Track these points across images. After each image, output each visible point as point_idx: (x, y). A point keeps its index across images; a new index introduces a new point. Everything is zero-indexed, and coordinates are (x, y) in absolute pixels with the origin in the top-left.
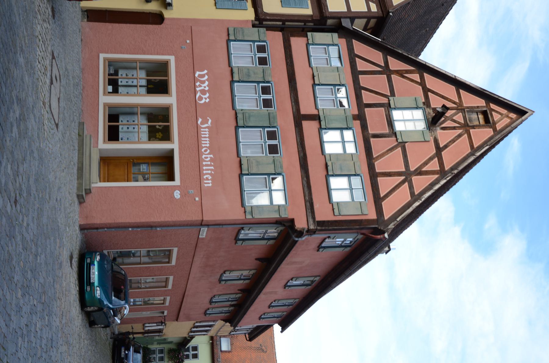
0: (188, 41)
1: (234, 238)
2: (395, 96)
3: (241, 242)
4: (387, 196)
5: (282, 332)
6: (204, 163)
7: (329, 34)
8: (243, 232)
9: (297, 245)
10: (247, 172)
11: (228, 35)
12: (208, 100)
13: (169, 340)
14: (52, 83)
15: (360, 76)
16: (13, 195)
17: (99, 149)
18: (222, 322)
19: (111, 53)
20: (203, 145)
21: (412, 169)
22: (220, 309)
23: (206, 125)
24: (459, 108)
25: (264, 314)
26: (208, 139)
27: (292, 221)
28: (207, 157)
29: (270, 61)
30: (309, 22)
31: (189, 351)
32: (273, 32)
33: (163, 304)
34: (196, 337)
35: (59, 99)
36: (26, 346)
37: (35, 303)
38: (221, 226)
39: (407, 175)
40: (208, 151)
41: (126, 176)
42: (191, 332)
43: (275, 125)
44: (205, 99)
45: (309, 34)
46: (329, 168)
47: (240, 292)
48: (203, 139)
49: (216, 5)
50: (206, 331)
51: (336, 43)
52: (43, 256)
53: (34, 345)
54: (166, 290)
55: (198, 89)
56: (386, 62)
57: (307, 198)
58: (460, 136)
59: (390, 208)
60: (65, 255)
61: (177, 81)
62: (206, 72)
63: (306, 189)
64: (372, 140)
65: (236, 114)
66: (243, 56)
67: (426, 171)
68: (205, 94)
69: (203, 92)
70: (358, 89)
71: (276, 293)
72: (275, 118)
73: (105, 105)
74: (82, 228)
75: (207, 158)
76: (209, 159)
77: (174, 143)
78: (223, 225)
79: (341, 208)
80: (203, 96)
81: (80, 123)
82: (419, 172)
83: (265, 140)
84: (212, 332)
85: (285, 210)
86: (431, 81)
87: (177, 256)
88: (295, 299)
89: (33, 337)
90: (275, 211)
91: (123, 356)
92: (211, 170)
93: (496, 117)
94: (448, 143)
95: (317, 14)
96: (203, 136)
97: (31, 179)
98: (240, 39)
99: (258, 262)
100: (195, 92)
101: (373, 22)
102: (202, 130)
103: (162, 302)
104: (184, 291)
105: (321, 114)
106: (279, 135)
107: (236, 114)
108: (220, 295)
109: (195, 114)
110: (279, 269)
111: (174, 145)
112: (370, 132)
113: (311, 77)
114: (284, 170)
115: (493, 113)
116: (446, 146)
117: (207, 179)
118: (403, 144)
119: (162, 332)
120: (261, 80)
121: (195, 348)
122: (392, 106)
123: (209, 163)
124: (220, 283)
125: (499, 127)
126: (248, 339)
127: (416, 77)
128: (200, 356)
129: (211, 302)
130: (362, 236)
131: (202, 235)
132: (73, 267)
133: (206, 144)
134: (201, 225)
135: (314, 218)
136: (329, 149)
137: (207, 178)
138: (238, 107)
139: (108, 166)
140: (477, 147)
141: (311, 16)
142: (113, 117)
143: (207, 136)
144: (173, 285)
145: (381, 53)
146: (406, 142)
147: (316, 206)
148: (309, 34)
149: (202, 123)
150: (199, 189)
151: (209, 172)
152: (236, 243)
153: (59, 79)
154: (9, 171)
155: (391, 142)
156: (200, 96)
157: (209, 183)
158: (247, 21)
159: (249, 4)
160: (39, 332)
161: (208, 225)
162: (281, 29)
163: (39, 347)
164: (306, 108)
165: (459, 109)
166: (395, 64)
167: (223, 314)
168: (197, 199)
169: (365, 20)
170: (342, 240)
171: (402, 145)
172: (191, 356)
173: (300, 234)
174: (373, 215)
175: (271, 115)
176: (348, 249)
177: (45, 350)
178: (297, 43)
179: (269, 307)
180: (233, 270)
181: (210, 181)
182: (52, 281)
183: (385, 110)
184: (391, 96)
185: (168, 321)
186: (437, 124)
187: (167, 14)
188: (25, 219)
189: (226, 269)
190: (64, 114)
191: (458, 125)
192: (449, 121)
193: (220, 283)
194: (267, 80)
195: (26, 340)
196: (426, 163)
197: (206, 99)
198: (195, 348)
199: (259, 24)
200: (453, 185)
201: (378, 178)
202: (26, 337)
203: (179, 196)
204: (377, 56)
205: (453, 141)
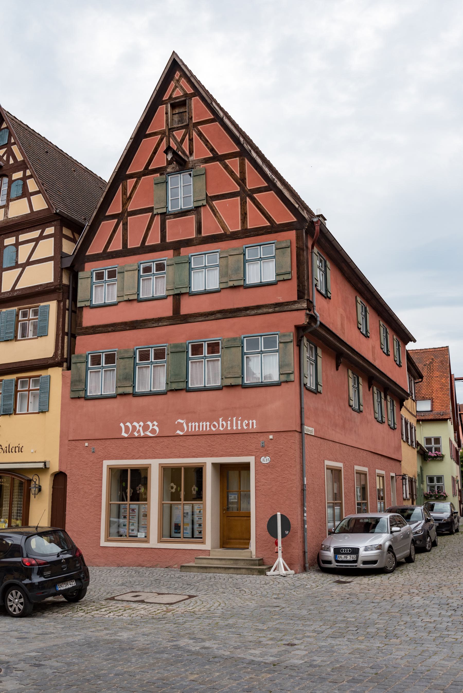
1: (315, 395)
2: (153, 207)
3: (319, 386)
4: (268, 218)
5: (415, 341)
6: (229, 428)
7: (80, 281)
8: (308, 385)
9: (323, 322)
12: (155, 423)
13: (419, 470)
14: (142, 602)
15: (129, 247)
16: (284, 648)
18: (403, 409)
19: (100, 533)
20: (208, 429)
21: (238, 189)
22: (389, 411)
23: (185, 425)
25: (395, 361)
27: (298, 328)
28: (222, 425)
29: (109, 351)
30: (65, 305)
31: (431, 448)
33: (383, 477)
34: (417, 439)
36: (453, 633)
37: (402, 623)
40: (215, 423)
41: (242, 518)
42: (412, 445)
44: (154, 426)
45: (79, 305)
46: (235, 285)
47: (371, 389)
49: (45, 412)
50: (411, 428)
51: (90, 274)
52: (347, 615)
53: (450, 624)
54: (369, 474)
55: (142, 434)
56: (113, 217)
57: (271, 310)
58: (200, 134)
59: (284, 216)
60: (336, 588)
61: (133, 458)
62: (122, 425)
63: (260, 311)
64: (203, 235)
65: (172, 390)
66: (101, 382)
67: (240, 173)
68: (148, 426)
69: (146, 428)
71: (373, 348)
72: (176, 346)
73: (160, 541)
74: (305, 569)
75: (223, 425)
76: (224, 423)
79: (283, 271)
80: (151, 428)
82: (241, 181)
84: (412, 420)
86: (136, 167)
88: (380, 325)
89: (441, 626)
90: (286, 347)
92: (237, 420)
93: (178, 93)
94: (208, 148)
95: (55, 295)
97: (260, 628)
99: (341, 367)
101: (66, 231)
102: (190, 430)
103: (381, 478)
104: (370, 453)
105: (171, 293)
106: (197, 341)
107: (172, 390)
108: (375, 412)
109: (172, 438)
110: (349, 343)
111: (208, 462)
112: (195, 237)
113: (129, 304)
114: (238, 336)
115: (174, 96)
116: (212, 150)
117: (248, 425)
118: (209, 199)
119: (412, 478)
121: (428, 440)
122: (164, 210)
123: (229, 422)
124: (362, 412)
125: (190, 91)
126: (420, 380)
128: (437, 435)
129: (382, 422)
130: (315, 247)
133: (206, 425)
134: (301, 432)
135: (294, 302)
136: (214, 284)
137: (246, 426)
138: (163, 387)
139: (231, 539)
140: (213, 115)
141: (59, 302)
144: (364, 466)
145: (102, 223)
147: (280, 299)
148: (79, 305)
149: (182, 430)
150: (259, 434)
151: (239, 422)
152: (320, 393)
153: (136, 593)
154: (257, 652)
155: (206, 213)
156: (149, 432)
157: (253, 423)
158: (63, 375)
160: (434, 618)
161: (302, 425)
162: (73, 337)
163: (451, 619)
164: (165, 309)
165: (169, 134)
166: (115, 207)
167: (395, 407)
168: (271, 437)
169: (64, 241)
170: (318, 270)
171: (210, 199)
172: (437, 446)
173: (313, 318)
175: (174, 350)
176: (328, 264)
177: (453, 612)
178: (89, 319)
179: (388, 355)
181: (251, 422)
182: (373, 604)
183: (169, 219)
185: (401, 472)
186: (186, 159)
187: (55, 468)
188: (308, 634)
189: (347, 405)
190: (176, 589)
191: (187, 136)
193: (362, 412)
194: (133, 355)
195: (447, 633)
196: (232, 173)
197: (154, 425)
200: (253, 143)
202: (443, 633)
203: (268, 457)
204: (106, 227)
205: (206, 142)
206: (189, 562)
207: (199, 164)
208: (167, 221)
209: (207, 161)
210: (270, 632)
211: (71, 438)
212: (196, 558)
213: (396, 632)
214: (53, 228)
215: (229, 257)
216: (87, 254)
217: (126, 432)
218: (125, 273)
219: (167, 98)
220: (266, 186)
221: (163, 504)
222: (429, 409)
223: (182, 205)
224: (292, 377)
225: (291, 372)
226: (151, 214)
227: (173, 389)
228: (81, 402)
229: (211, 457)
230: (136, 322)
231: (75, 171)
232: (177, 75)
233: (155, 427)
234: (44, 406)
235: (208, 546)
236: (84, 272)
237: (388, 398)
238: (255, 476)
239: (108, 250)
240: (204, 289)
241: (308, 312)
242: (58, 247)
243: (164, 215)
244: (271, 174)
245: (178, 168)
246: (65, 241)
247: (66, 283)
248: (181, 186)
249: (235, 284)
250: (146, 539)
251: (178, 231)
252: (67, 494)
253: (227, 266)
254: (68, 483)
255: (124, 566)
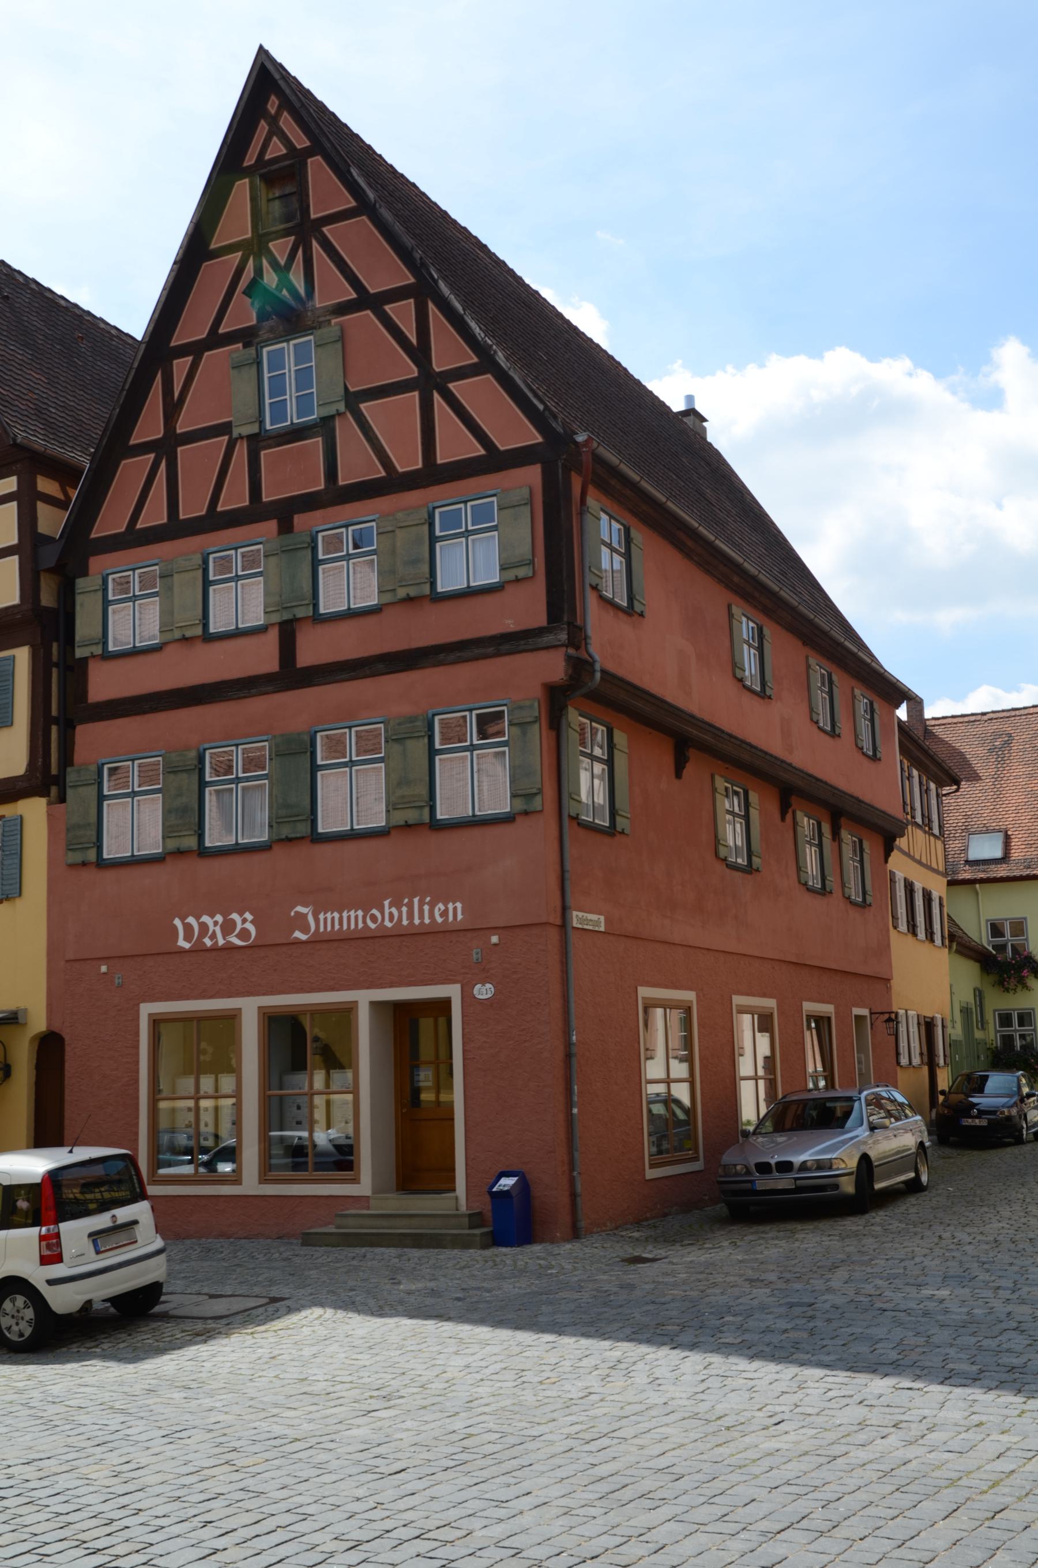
0: (104, 969)
2: (230, 423)
6: (405, 922)
7: (79, 599)
10: (426, 811)
11: (84, 864)
12: (248, 916)
15: (181, 517)
17: (373, 1193)
18: (895, 857)
20: (361, 925)
21: (414, 372)
23: (311, 919)
24: (255, 250)
26: (345, 914)
28: (389, 916)
32: (76, 747)
35: (212, 1296)
38: (567, 875)
39: (430, 383)
40: (374, 911)
43: (307, 738)
44: (245, 922)
45: (79, 653)
46: (412, 594)
47: (789, 816)
48: (345, 927)
55: (221, 942)
57: (490, 650)
61: (204, 995)
62: (177, 922)
68: (233, 923)
69: (228, 927)
70: (215, 521)
73: (264, 1179)
75: (391, 915)
76: (394, 910)
77: (356, 1002)
78: (563, 871)
81: (305, 1244)
82: (420, 353)
83: (231, 782)
85: (521, 708)
86: (191, 329)
87: (666, 987)
90: (524, 733)
91: (984, 1123)
92: (421, 904)
93: (277, 149)
96: (337, 927)
98: (94, 833)
99: (689, 770)
100: (230, 948)
101: (46, 485)
102: (322, 929)
105: (276, 618)
111: (249, 1009)
117: (444, 914)
120: (195, 778)
122: (254, 429)
123: (404, 909)
125: (302, 142)
127: (181, 366)
128: (1017, 914)
131: (597, 923)
132: (664, 1254)
133: (356, 917)
134: (564, 925)
135: (540, 632)
137: (441, 915)
138: (263, 836)
142: (299, 1158)
143: (336, 915)
144: (764, 995)
145: (123, 462)
146: (346, 388)
147: (510, 625)
148: (79, 653)
149: (305, 929)
151: (426, 908)
155: (346, 431)
156: (237, 936)
157: (455, 909)
158: (50, 816)
159: (6, 810)
161: (565, 910)
162: (68, 727)
164: (262, 656)
166: (149, 427)
168: (495, 939)
169: (41, 506)
171: (353, 400)
174: (532, 475)
178: (104, 684)
180: (716, 836)
181: (451, 906)
183: (266, 448)
184: (230, 433)
187: (38, 1023)
191: (300, 252)
192: (291, 276)
194: (195, 762)
197: (244, 921)
198: (996, 930)
199: (56, 784)
201: (439, 461)
203: (489, 986)
204: (132, 471)
206: (326, 1224)
207: (328, 318)
208: (262, 453)
209: (343, 309)
210: (368, 1374)
211: (70, 956)
212: (337, 1215)
213: (951, 1366)
214: (14, 479)
215: (398, 531)
216: (93, 536)
217: (186, 939)
218: (176, 576)
219: (253, 162)
220: (474, 364)
221: (269, 1096)
222: (998, 854)
223: (293, 417)
224: (537, 803)
225: (535, 791)
226: (226, 438)
227: (283, 837)
228: (89, 875)
229: (368, 988)
230: (203, 687)
231: (82, 338)
232: (273, 105)
233: (249, 926)
234: (11, 884)
235: (364, 1187)
236: (88, 578)
237: (846, 836)
238: (463, 1029)
239: (138, 526)
240: (346, 608)
241: (571, 651)
242: (27, 521)
243: (257, 442)
244: (483, 335)
245: (281, 327)
246: (42, 508)
247: (50, 605)
248: (290, 371)
249: (416, 592)
250: (235, 1179)
251: (290, 474)
252: (66, 1082)
253: (393, 552)
254: (67, 1058)
255: (188, 1237)
